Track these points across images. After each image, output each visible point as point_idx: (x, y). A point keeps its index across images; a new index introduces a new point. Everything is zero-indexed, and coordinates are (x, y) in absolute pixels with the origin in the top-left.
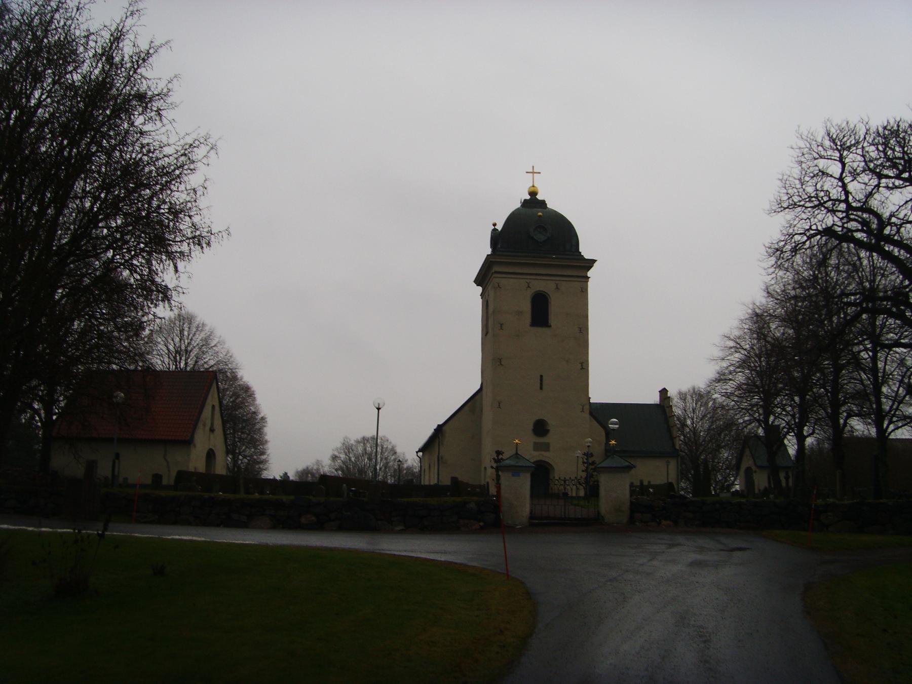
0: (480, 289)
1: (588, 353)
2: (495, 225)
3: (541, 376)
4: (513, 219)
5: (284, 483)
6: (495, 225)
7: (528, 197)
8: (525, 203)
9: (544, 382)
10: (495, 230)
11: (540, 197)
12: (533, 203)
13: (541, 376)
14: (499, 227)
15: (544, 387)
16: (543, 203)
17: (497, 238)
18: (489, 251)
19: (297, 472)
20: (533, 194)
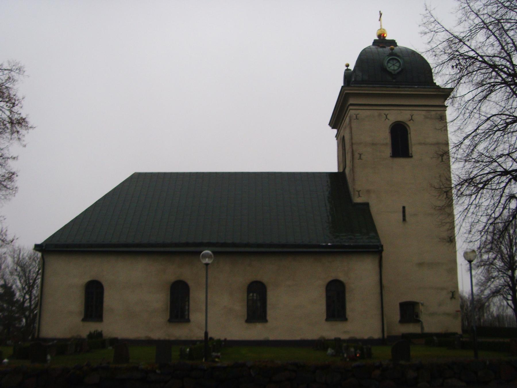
0: (335, 131)
1: (165, 174)
2: (347, 66)
3: (404, 208)
4: (364, 58)
5: (46, 340)
6: (347, 66)
7: (377, 38)
8: (375, 43)
9: (401, 215)
10: (347, 70)
11: (388, 37)
12: (381, 41)
13: (404, 208)
14: (352, 67)
15: (407, 218)
16: (393, 43)
17: (348, 77)
18: (342, 84)
19: (97, 331)
20: (455, 298)
